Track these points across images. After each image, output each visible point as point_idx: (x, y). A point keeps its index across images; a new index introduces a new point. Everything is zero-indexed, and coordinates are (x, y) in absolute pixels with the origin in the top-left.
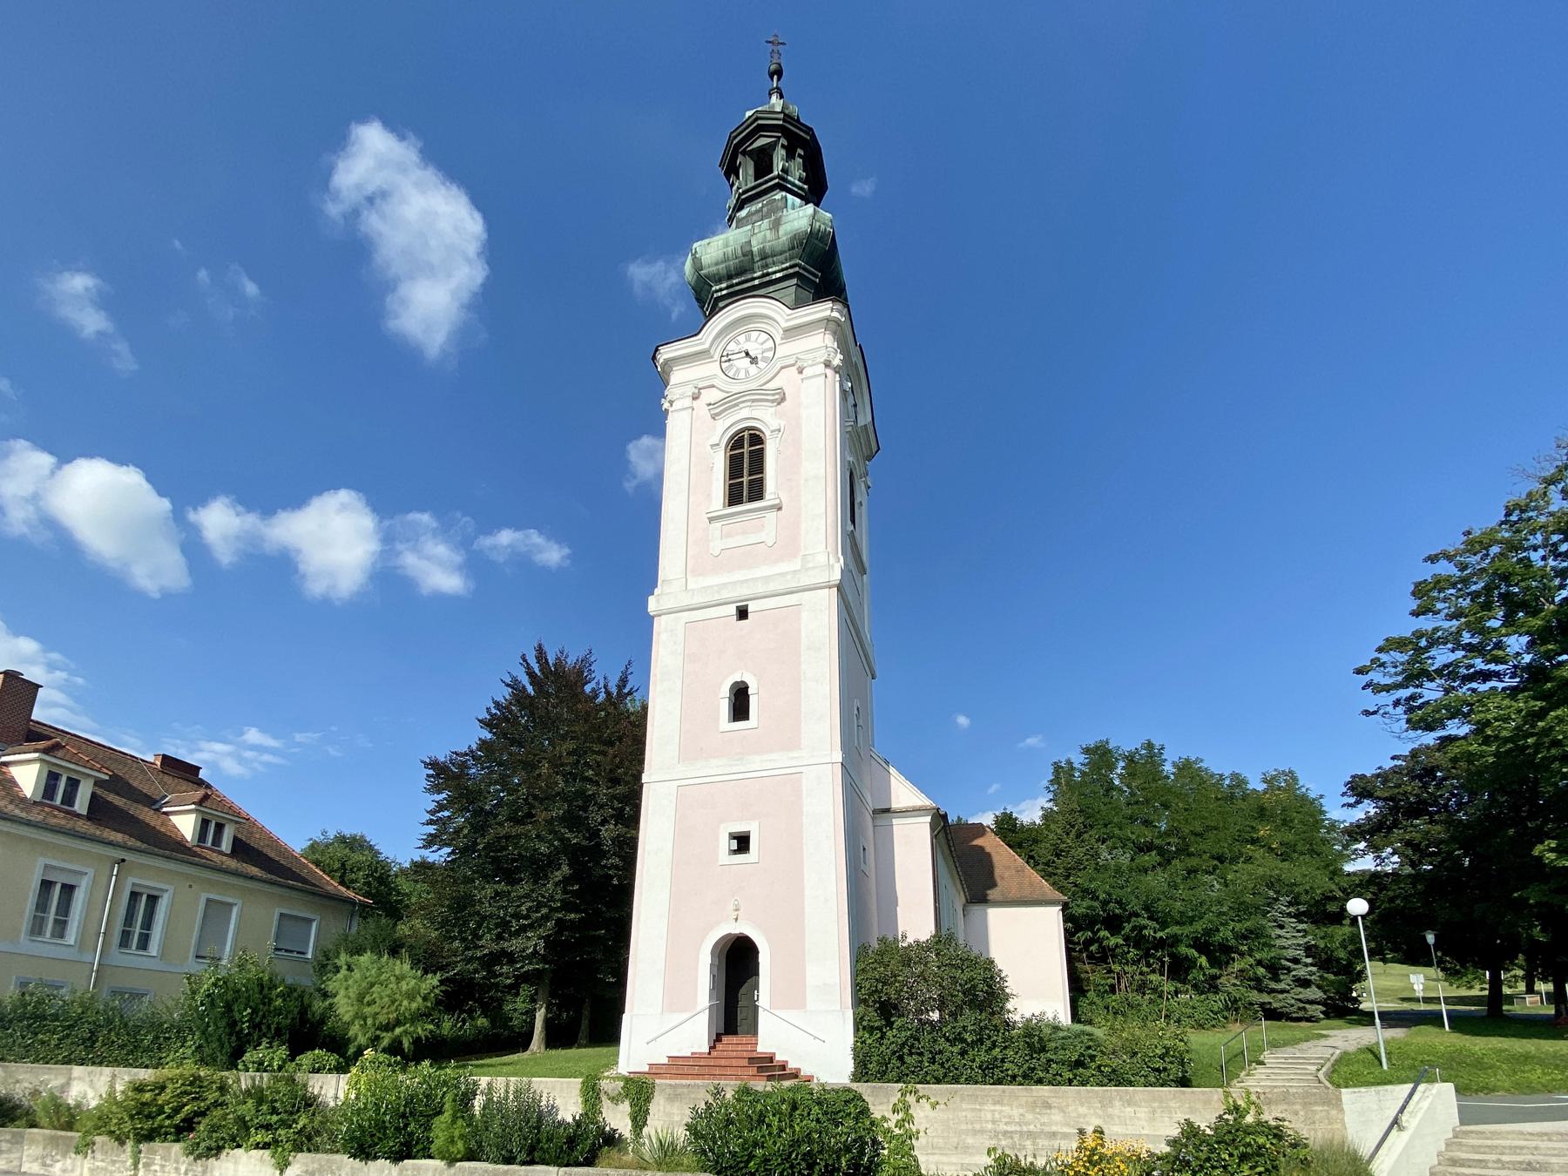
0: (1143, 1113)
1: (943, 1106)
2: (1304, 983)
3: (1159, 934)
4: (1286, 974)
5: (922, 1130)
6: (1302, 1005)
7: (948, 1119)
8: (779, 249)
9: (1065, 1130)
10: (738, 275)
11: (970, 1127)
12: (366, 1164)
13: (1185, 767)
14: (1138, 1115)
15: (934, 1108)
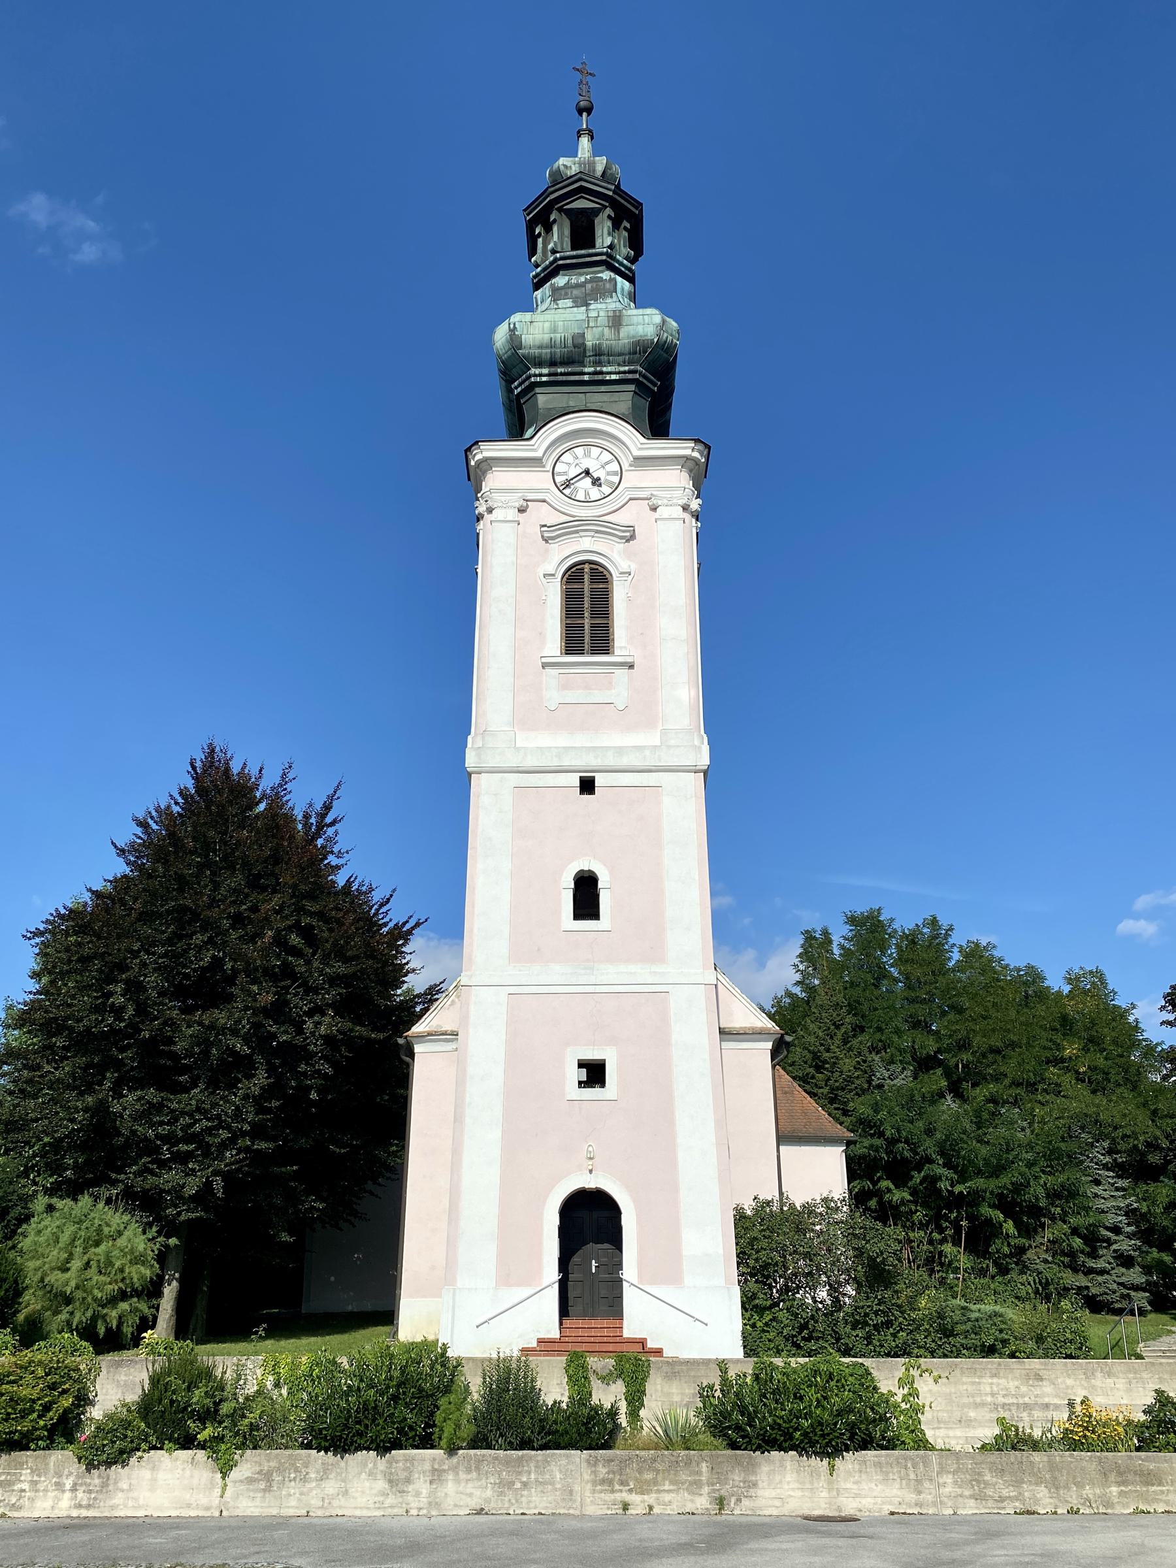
0: (1121, 1383)
1: (945, 1380)
2: (1126, 1261)
3: (958, 1189)
4: (1105, 1247)
5: (927, 1404)
6: (1125, 1291)
7: (950, 1394)
8: (618, 349)
9: (1056, 1401)
10: (563, 363)
11: (971, 1400)
12: (342, 1458)
13: (975, 954)
14: (1117, 1386)
15: (936, 1382)
